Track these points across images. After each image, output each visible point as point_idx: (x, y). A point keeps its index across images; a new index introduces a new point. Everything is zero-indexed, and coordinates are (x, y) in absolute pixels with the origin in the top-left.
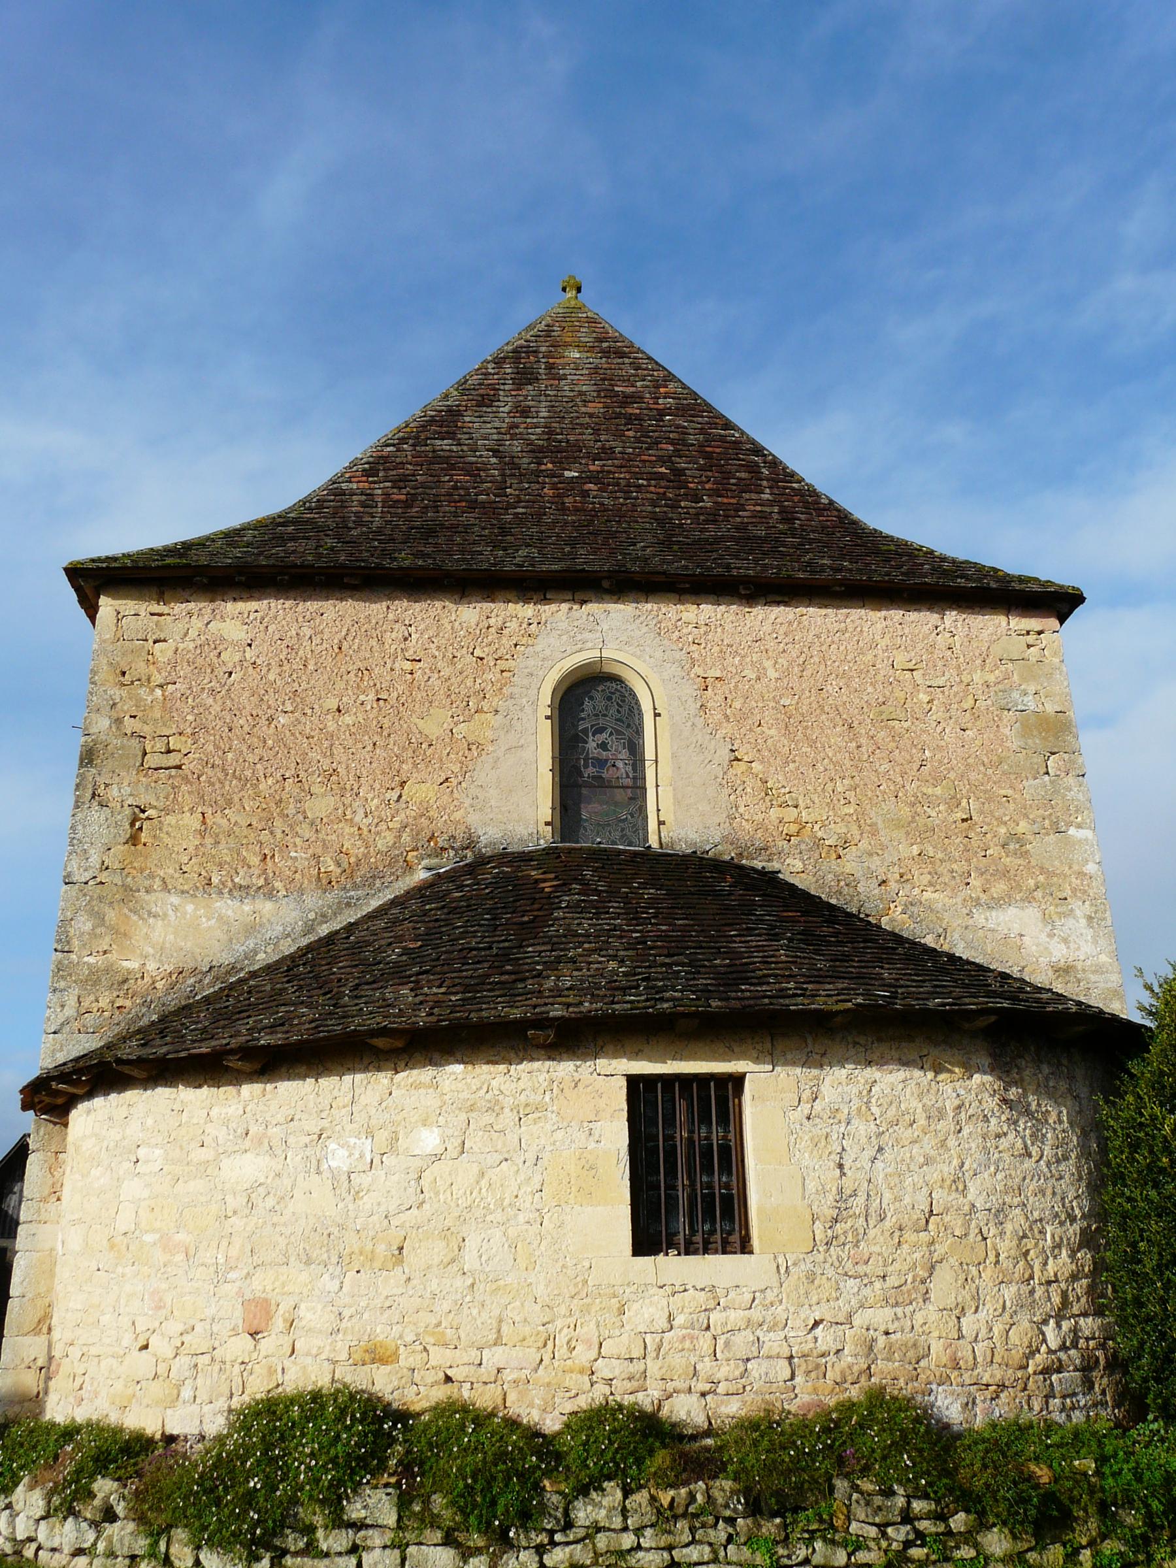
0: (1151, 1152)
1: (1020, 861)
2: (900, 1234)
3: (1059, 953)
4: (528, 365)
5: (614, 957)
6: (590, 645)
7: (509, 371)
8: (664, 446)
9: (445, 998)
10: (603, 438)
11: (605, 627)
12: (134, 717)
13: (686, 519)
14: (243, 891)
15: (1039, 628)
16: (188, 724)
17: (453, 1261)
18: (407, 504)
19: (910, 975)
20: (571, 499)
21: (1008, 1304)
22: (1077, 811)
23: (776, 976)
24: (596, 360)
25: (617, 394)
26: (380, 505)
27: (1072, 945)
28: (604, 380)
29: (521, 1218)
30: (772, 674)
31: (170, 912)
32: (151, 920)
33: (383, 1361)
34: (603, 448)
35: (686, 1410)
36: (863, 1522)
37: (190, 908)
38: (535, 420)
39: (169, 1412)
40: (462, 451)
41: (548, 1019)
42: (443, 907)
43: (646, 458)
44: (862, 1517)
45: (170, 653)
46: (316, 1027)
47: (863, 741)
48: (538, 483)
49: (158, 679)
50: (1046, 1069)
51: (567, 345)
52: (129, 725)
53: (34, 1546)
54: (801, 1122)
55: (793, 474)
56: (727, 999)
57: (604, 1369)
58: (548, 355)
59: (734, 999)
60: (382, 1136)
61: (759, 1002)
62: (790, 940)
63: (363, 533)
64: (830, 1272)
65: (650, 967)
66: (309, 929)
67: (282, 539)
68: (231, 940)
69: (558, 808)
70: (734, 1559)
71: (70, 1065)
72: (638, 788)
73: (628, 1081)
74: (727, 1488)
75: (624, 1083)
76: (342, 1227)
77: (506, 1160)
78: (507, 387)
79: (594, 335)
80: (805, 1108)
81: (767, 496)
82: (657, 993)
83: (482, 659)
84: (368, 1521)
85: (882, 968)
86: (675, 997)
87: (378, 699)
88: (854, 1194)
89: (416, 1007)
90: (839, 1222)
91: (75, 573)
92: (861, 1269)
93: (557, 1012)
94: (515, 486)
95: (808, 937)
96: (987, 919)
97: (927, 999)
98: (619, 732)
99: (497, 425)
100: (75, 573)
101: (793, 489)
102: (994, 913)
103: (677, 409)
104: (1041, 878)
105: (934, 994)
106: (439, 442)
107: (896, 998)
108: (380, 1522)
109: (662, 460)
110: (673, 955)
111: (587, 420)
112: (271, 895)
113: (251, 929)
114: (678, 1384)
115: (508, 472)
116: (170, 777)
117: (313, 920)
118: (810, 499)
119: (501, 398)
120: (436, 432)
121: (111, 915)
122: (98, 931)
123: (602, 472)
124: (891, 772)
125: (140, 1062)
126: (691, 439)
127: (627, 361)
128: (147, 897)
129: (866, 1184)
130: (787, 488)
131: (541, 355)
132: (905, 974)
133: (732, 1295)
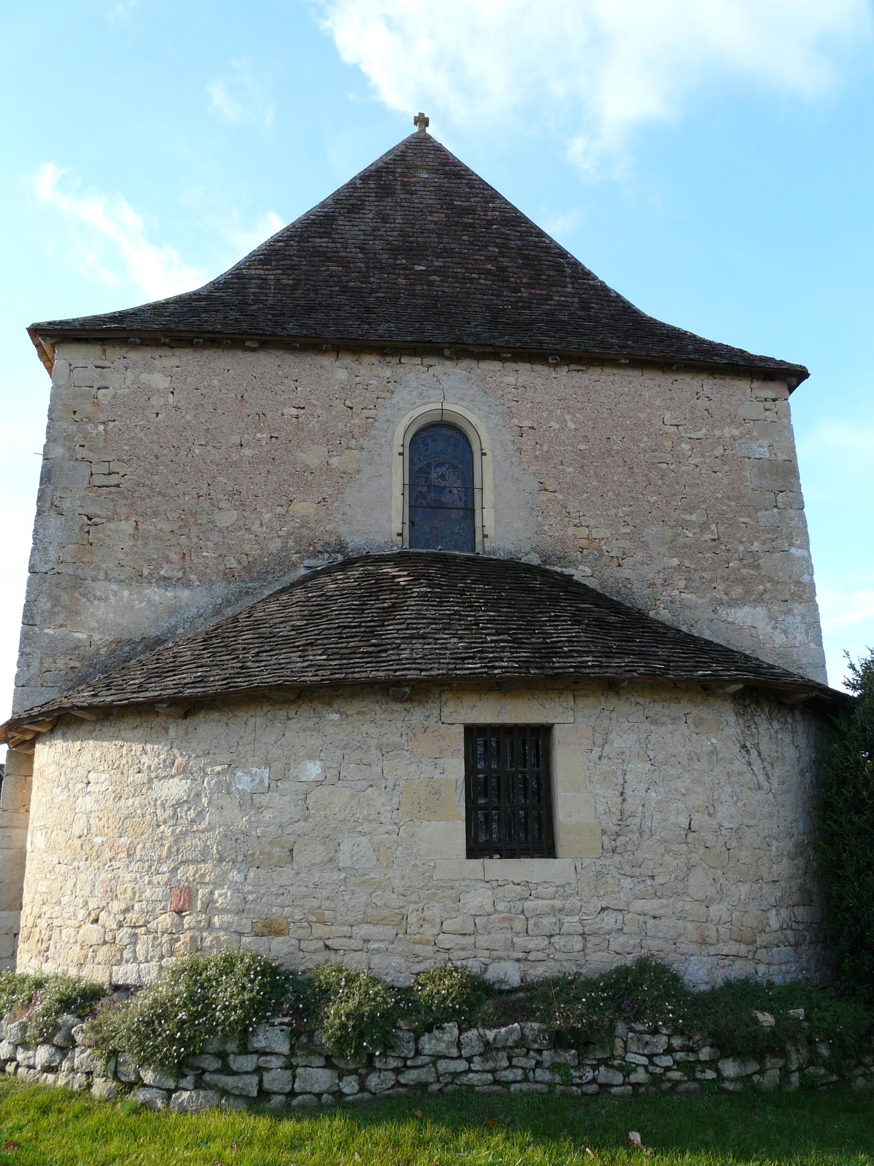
0: (854, 787)
1: (752, 572)
2: (671, 845)
3: (779, 639)
4: (387, 182)
5: (454, 635)
6: (433, 399)
7: (373, 186)
8: (491, 249)
9: (326, 663)
10: (445, 241)
11: (446, 387)
12: (83, 446)
13: (508, 305)
14: (166, 582)
15: (774, 397)
16: (124, 452)
17: (331, 860)
18: (294, 287)
19: (679, 653)
20: (419, 287)
21: (743, 897)
22: (797, 536)
23: (578, 651)
24: (438, 180)
25: (456, 207)
26: (272, 287)
27: (790, 636)
28: (446, 195)
29: (382, 830)
30: (571, 425)
31: (111, 596)
32: (96, 602)
33: (279, 933)
34: (445, 248)
35: (508, 973)
36: (635, 1053)
37: (126, 593)
38: (392, 225)
39: (115, 968)
40: (337, 247)
41: (405, 680)
42: (322, 595)
43: (478, 257)
44: (635, 1049)
45: (109, 398)
46: (228, 683)
47: (640, 478)
48: (395, 274)
49: (102, 417)
50: (776, 725)
51: (417, 167)
52: (81, 453)
53: (14, 1064)
54: (612, 764)
55: (589, 273)
56: (542, 668)
57: (446, 941)
58: (403, 175)
59: (547, 668)
60: (278, 766)
61: (566, 670)
62: (587, 625)
63: (260, 309)
64: (615, 872)
65: (483, 643)
66: (217, 612)
67: (196, 312)
68: (157, 619)
69: (408, 523)
70: (539, 1079)
71: (36, 710)
72: (469, 511)
73: (465, 728)
74: (536, 1028)
75: (462, 730)
76: (246, 834)
77: (371, 786)
78: (371, 199)
79: (439, 160)
80: (597, 751)
81: (569, 290)
82: (489, 662)
83: (351, 408)
84: (267, 1050)
85: (657, 647)
86: (505, 665)
87: (272, 437)
88: (633, 815)
89: (303, 670)
90: (618, 836)
91: (37, 332)
92: (637, 871)
93: (412, 675)
94: (377, 276)
95: (600, 624)
96: (728, 615)
97: (693, 671)
98: (455, 467)
99: (363, 228)
100: (37, 332)
101: (590, 285)
102: (733, 611)
103: (501, 220)
104: (768, 585)
105: (697, 667)
106: (319, 240)
107: (669, 670)
108: (277, 1050)
109: (489, 259)
110: (500, 634)
111: (433, 226)
112: (188, 585)
113: (172, 611)
114: (501, 953)
115: (371, 265)
116: (111, 493)
117: (220, 605)
118: (602, 293)
119: (367, 207)
120: (316, 232)
121: (65, 597)
122: (56, 609)
123: (444, 267)
124: (660, 503)
125: (90, 708)
126: (513, 244)
127: (464, 181)
128: (93, 585)
129: (641, 808)
130: (585, 284)
131: (397, 175)
132: (675, 653)
133: (540, 889)
